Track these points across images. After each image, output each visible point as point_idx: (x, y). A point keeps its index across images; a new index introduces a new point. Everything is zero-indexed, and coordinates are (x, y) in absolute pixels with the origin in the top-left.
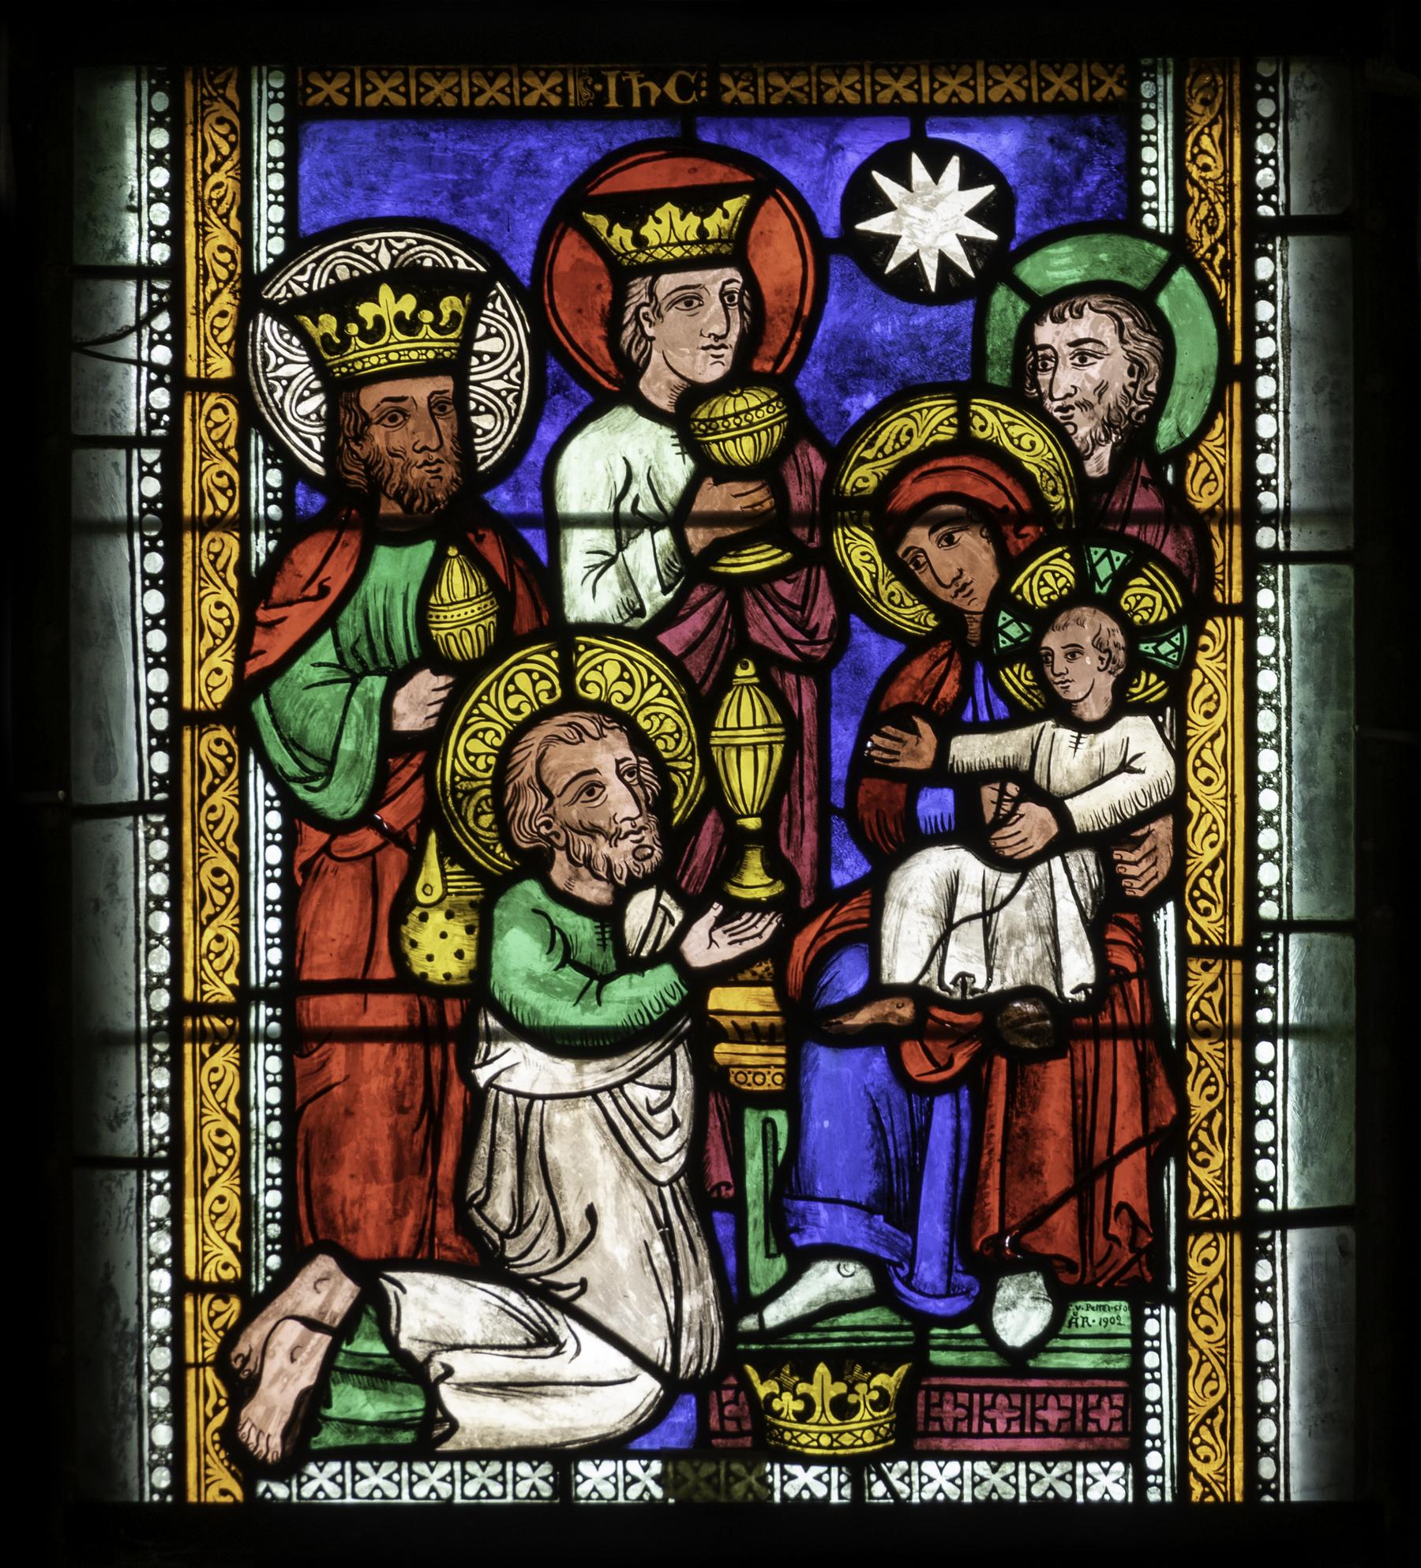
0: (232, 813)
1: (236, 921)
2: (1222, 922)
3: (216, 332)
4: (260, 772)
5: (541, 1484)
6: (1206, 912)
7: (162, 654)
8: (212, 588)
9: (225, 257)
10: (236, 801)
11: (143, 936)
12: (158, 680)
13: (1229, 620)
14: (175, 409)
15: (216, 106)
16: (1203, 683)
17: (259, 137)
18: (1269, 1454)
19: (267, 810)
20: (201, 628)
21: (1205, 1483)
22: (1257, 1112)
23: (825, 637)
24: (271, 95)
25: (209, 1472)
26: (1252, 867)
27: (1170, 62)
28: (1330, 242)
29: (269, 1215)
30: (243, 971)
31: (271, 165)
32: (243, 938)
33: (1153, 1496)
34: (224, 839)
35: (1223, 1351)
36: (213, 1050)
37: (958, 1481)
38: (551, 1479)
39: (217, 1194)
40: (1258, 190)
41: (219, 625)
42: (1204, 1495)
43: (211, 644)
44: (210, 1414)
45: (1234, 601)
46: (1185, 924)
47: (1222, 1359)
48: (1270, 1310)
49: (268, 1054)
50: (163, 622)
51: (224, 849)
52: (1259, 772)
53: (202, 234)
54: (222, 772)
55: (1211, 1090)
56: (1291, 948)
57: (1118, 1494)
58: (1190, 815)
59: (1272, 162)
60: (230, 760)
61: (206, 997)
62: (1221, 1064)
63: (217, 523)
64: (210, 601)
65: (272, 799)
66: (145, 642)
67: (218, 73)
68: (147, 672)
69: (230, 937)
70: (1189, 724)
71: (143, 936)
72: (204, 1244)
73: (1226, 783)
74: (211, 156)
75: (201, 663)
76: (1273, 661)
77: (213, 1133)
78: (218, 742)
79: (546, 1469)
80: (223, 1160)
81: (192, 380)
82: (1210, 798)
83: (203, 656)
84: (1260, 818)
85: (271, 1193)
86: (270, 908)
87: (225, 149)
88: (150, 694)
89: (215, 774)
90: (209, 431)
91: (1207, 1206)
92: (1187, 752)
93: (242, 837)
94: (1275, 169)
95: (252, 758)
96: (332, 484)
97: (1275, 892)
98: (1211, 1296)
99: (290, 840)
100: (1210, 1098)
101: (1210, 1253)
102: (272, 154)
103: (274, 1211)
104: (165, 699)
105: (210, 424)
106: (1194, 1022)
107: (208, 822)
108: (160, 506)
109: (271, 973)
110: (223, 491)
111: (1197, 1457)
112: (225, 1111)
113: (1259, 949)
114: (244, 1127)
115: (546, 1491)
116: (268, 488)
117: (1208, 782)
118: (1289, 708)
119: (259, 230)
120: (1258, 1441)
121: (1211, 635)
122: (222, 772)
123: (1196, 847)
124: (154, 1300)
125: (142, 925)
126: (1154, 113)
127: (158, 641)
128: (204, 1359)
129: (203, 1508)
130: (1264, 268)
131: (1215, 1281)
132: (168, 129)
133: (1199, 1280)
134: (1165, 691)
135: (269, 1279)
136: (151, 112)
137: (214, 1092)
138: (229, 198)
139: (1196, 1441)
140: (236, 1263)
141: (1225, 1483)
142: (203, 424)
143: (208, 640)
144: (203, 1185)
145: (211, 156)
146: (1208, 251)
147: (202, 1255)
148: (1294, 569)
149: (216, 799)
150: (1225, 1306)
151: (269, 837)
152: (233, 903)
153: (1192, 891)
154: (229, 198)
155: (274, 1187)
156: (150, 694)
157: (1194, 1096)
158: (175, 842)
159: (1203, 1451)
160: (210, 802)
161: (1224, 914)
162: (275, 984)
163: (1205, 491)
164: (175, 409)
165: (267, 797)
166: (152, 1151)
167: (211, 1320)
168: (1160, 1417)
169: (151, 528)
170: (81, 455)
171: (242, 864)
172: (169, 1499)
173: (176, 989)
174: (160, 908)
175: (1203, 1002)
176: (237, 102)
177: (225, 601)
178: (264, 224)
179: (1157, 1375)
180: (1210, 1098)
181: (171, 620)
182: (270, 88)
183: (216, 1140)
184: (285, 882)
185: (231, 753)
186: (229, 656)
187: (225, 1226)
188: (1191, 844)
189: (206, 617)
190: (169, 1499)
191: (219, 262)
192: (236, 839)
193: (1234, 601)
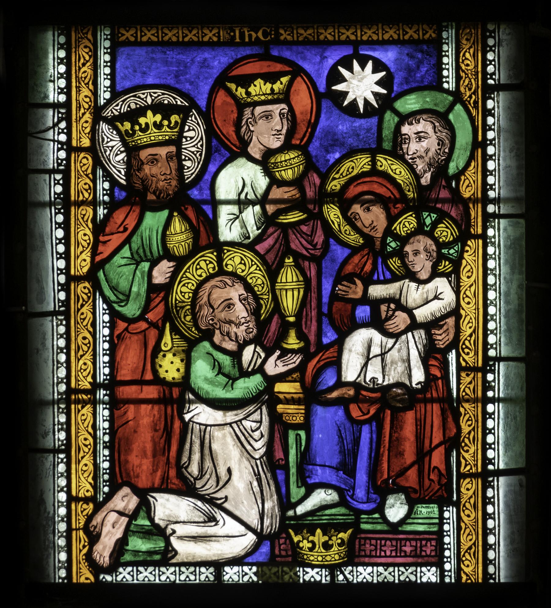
0: (90, 315)
1: (92, 357)
2: (474, 358)
4: (101, 299)
5: (210, 575)
6: (468, 354)
7: (63, 253)
8: (82, 228)
9: (87, 100)
10: (92, 310)
11: (55, 363)
12: (61, 264)
13: (477, 241)
14: (68, 159)
15: (84, 41)
16: (467, 265)
17: (100, 53)
19: (104, 314)
20: (78, 244)
21: (467, 575)
22: (488, 431)
23: (320, 247)
24: (105, 37)
25: (81, 571)
27: (454, 24)
28: (516, 94)
29: (104, 471)
30: (94, 377)
31: (105, 64)
32: (94, 364)
33: (447, 580)
34: (87, 325)
35: (474, 524)
36: (83, 407)
37: (372, 574)
38: (214, 574)
39: (84, 463)
40: (488, 74)
41: (85, 242)
42: (467, 580)
43: (82, 250)
44: (81, 548)
45: (479, 233)
46: (460, 358)
47: (474, 527)
48: (493, 508)
49: (104, 409)
50: (63, 241)
51: (87, 329)
52: (488, 299)
53: (78, 91)
54: (86, 299)
55: (470, 423)
56: (501, 367)
57: (434, 579)
58: (461, 316)
59: (493, 63)
60: (89, 295)
61: (80, 387)
62: (474, 413)
63: (84, 203)
64: (81, 233)
66: (56, 249)
67: (84, 28)
68: (57, 261)
69: (89, 363)
70: (461, 281)
71: (55, 363)
72: (79, 482)
73: (475, 303)
74: (82, 61)
75: (78, 257)
76: (493, 256)
77: (83, 439)
78: (85, 288)
79: (212, 570)
80: (86, 450)
81: (75, 147)
82: (469, 309)
83: (79, 254)
85: (105, 463)
86: (105, 352)
87: (87, 58)
88: (58, 269)
89: (84, 300)
90: (81, 167)
91: (468, 468)
92: (460, 292)
93: (94, 324)
94: (495, 66)
95: (98, 294)
96: (129, 188)
97: (494, 346)
98: (469, 502)
99: (112, 326)
100: (469, 426)
101: (469, 486)
102: (106, 60)
103: (106, 469)
104: (64, 271)
105: (82, 164)
106: (463, 396)
107: (81, 319)
110: (86, 190)
111: (464, 565)
112: (87, 431)
113: (488, 368)
114: (95, 437)
115: (212, 578)
116: (104, 189)
117: (469, 303)
118: (500, 275)
119: (100, 89)
120: (488, 559)
121: (469, 246)
122: (86, 299)
123: (464, 329)
124: (60, 504)
125: (55, 359)
126: (448, 44)
127: (61, 248)
128: (79, 527)
129: (79, 585)
130: (490, 104)
131: (471, 497)
132: (65, 50)
133: (465, 496)
134: (452, 268)
135: (104, 496)
136: (59, 43)
137: (83, 423)
138: (89, 77)
139: (464, 559)
140: (91, 490)
141: (475, 575)
142: (79, 164)
143: (81, 248)
144: (79, 459)
145: (82, 61)
146: (468, 97)
147: (78, 487)
148: (502, 221)
149: (84, 310)
150: (475, 507)
151: (104, 324)
152: (90, 350)
153: (462, 345)
154: (89, 77)
155: (106, 460)
156: (58, 269)
157: (463, 425)
158: (68, 327)
159: (466, 563)
160: (81, 311)
161: (475, 354)
162: (107, 382)
163: (467, 190)
164: (68, 159)
165: (104, 309)
166: (59, 446)
167: (82, 512)
168: (450, 549)
170: (31, 176)
171: (94, 335)
172: (66, 581)
173: (68, 384)
174: (62, 352)
175: (466, 388)
176: (92, 40)
177: (87, 233)
178: (102, 87)
179: (449, 533)
180: (469, 426)
181: (66, 240)
182: (105, 34)
183: (84, 442)
184: (111, 342)
185: (90, 292)
186: (89, 254)
187: (87, 475)
188: (462, 327)
189: (80, 239)
190: (66, 581)
191: (85, 102)
192: (91, 325)
193: (479, 233)
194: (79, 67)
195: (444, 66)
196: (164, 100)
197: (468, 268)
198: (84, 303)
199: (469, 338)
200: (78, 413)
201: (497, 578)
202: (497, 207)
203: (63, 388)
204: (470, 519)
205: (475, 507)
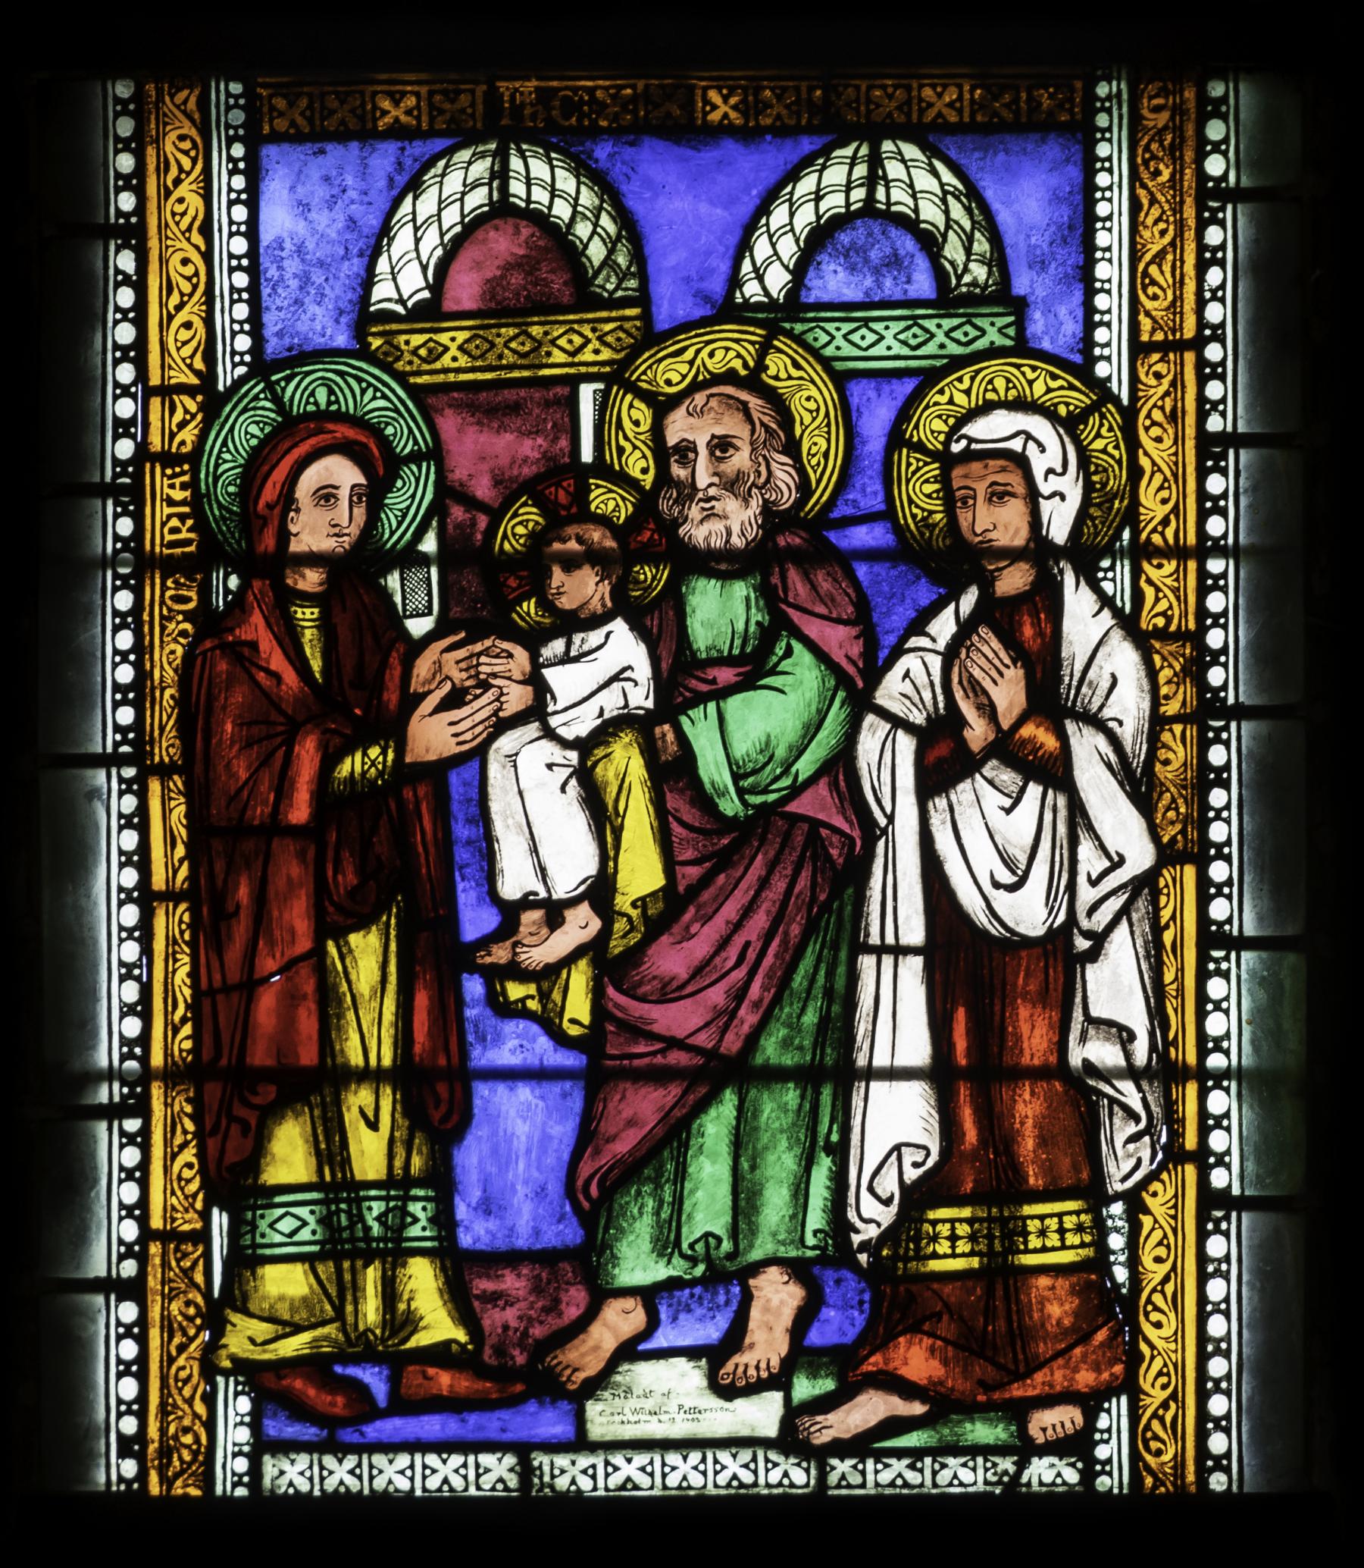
0: (195, 202)
3: (183, 1183)
5: (507, 1476)
6: (1158, 1453)
13: (1179, 1168)
16: (1153, 1229)
18: (1219, 1311)
22: (1213, 852)
26: (1202, 1436)
32: (207, 198)
33: (1103, 1483)
35: (169, 242)
38: (518, 1468)
40: (1209, 1000)
42: (1155, 1487)
45: (1188, 543)
46: (1139, 578)
48: (1225, 752)
50: (137, 934)
55: (1165, 494)
58: (1142, 1358)
59: (1226, 890)
62: (1173, 1222)
64: (177, 258)
65: (244, 1384)
67: (180, 90)
68: (120, 869)
69: (198, 324)
76: (1223, 1306)
79: (510, 1460)
83: (177, 864)
84: (1210, 1385)
88: (121, 889)
89: (1162, 1420)
92: (1140, 1417)
93: (206, 230)
97: (1224, 1385)
98: (1163, 1292)
108: (131, 508)
109: (238, 1419)
115: (513, 1481)
117: (1159, 440)
119: (220, 230)
121: (1163, 1182)
123: (1146, 1386)
124: (1223, 1306)
126: (1109, 111)
130: (1216, 1246)
141: (1176, 1351)
143: (175, 300)
145: (174, 172)
148: (1245, 955)
149: (183, 190)
150: (1176, 1302)
151: (1106, 318)
153: (1145, 1307)
156: (121, 889)
161: (1176, 442)
169: (125, 564)
171: (207, 256)
172: (136, 1486)
175: (1155, 410)
180: (1164, 501)
181: (140, 287)
187: (190, 353)
190: (136, 1486)
191: (182, 275)
194: (168, 312)
195: (241, 132)
196: (387, 424)
197: (1157, 1235)
198: (1161, 1412)
199: (1160, 529)
200: (166, 198)
201: (1232, 111)
202: (1231, 86)
203: (125, 449)
204: (1161, 446)
205: (1173, 417)
